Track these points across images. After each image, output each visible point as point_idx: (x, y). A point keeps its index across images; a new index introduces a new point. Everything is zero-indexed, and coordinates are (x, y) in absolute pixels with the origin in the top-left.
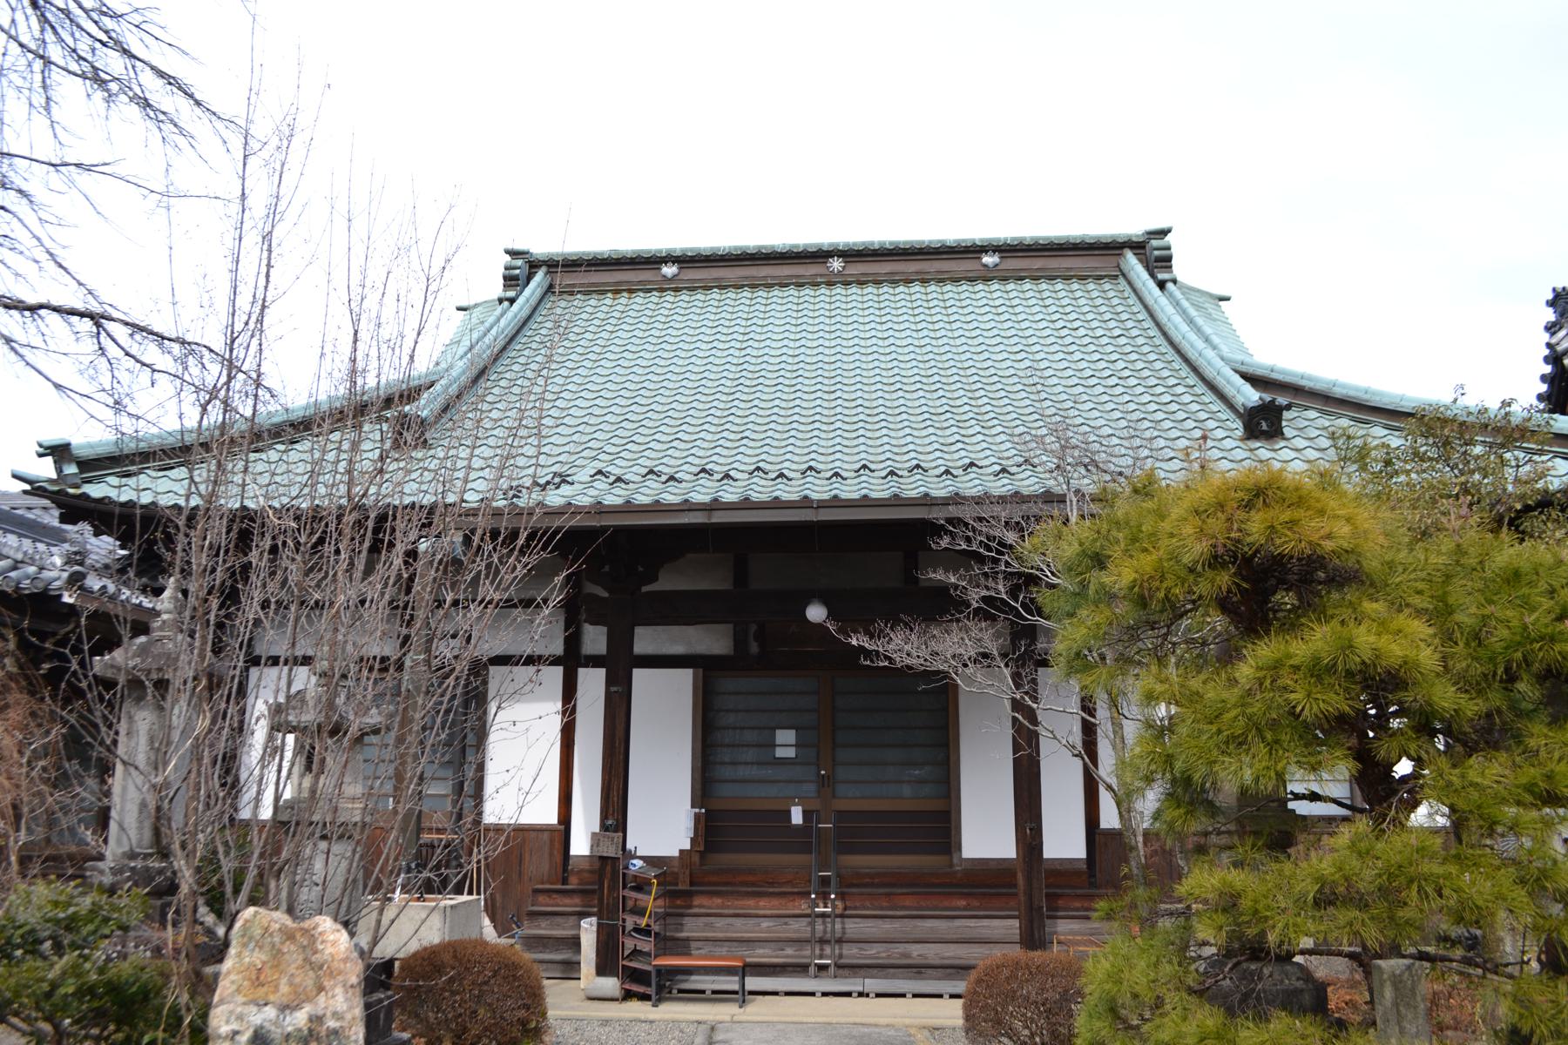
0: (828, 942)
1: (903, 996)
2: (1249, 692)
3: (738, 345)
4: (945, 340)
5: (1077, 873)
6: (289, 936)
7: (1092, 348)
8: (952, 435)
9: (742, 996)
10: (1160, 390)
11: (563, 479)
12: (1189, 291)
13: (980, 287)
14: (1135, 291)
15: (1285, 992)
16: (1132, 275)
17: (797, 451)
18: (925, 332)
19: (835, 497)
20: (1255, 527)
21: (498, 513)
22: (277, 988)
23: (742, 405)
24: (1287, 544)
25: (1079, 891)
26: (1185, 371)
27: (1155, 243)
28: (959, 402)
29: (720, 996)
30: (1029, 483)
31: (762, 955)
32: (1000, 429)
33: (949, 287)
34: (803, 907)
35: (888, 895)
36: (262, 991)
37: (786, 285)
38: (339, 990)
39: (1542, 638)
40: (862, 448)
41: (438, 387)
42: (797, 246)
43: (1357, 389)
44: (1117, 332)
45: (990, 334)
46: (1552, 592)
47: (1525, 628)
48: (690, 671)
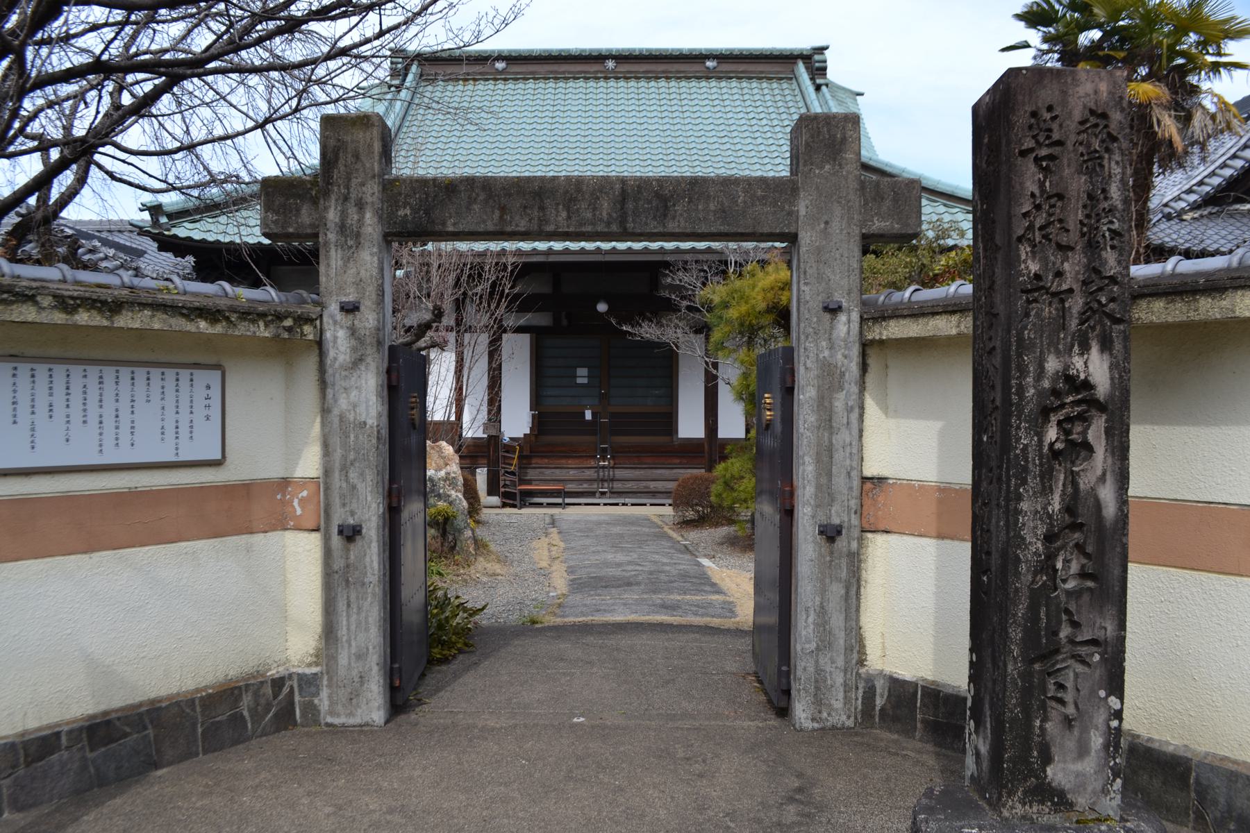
16: (800, 79)
27: (817, 57)
31: (570, 487)
34: (593, 463)
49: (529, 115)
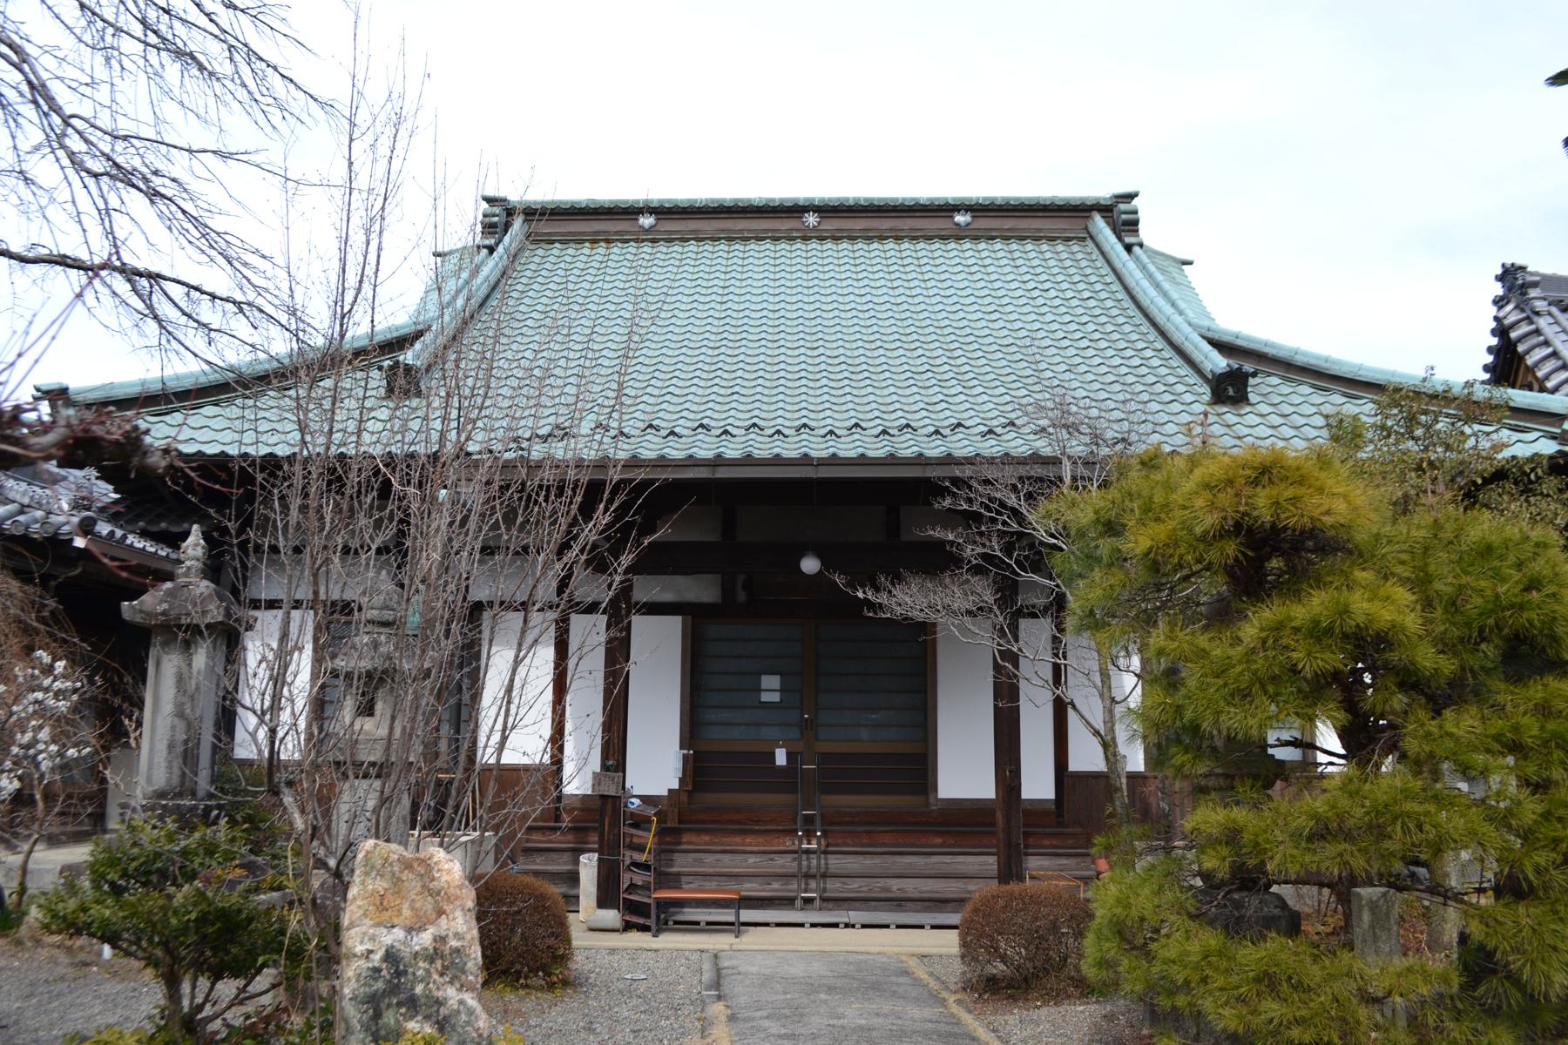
0: (814, 877)
1: (887, 926)
2: (1253, 651)
3: (719, 299)
4: (921, 299)
5: (1045, 813)
6: (408, 865)
7: (1064, 310)
8: (935, 395)
9: (737, 927)
10: (1129, 353)
11: (566, 434)
12: (1154, 254)
13: (953, 245)
14: (1103, 253)
15: (1265, 918)
16: (1100, 238)
17: (788, 407)
18: (901, 290)
19: (834, 455)
20: (1262, 504)
21: (508, 466)
22: (400, 912)
23: (728, 360)
24: (1291, 518)
25: (1048, 830)
26: (1153, 335)
27: (1122, 207)
28: (938, 362)
29: (714, 927)
30: (1018, 445)
31: (751, 889)
32: (981, 390)
33: (922, 245)
34: (788, 843)
35: (868, 832)
36: (386, 915)
37: (763, 239)
38: (458, 913)
39: (1512, 606)
40: (850, 406)
41: (428, 337)
42: (773, 200)
43: (1318, 357)
44: (1086, 295)
45: (965, 293)
46: (1519, 565)
47: (1497, 597)
48: (680, 618)
49: (688, 284)
